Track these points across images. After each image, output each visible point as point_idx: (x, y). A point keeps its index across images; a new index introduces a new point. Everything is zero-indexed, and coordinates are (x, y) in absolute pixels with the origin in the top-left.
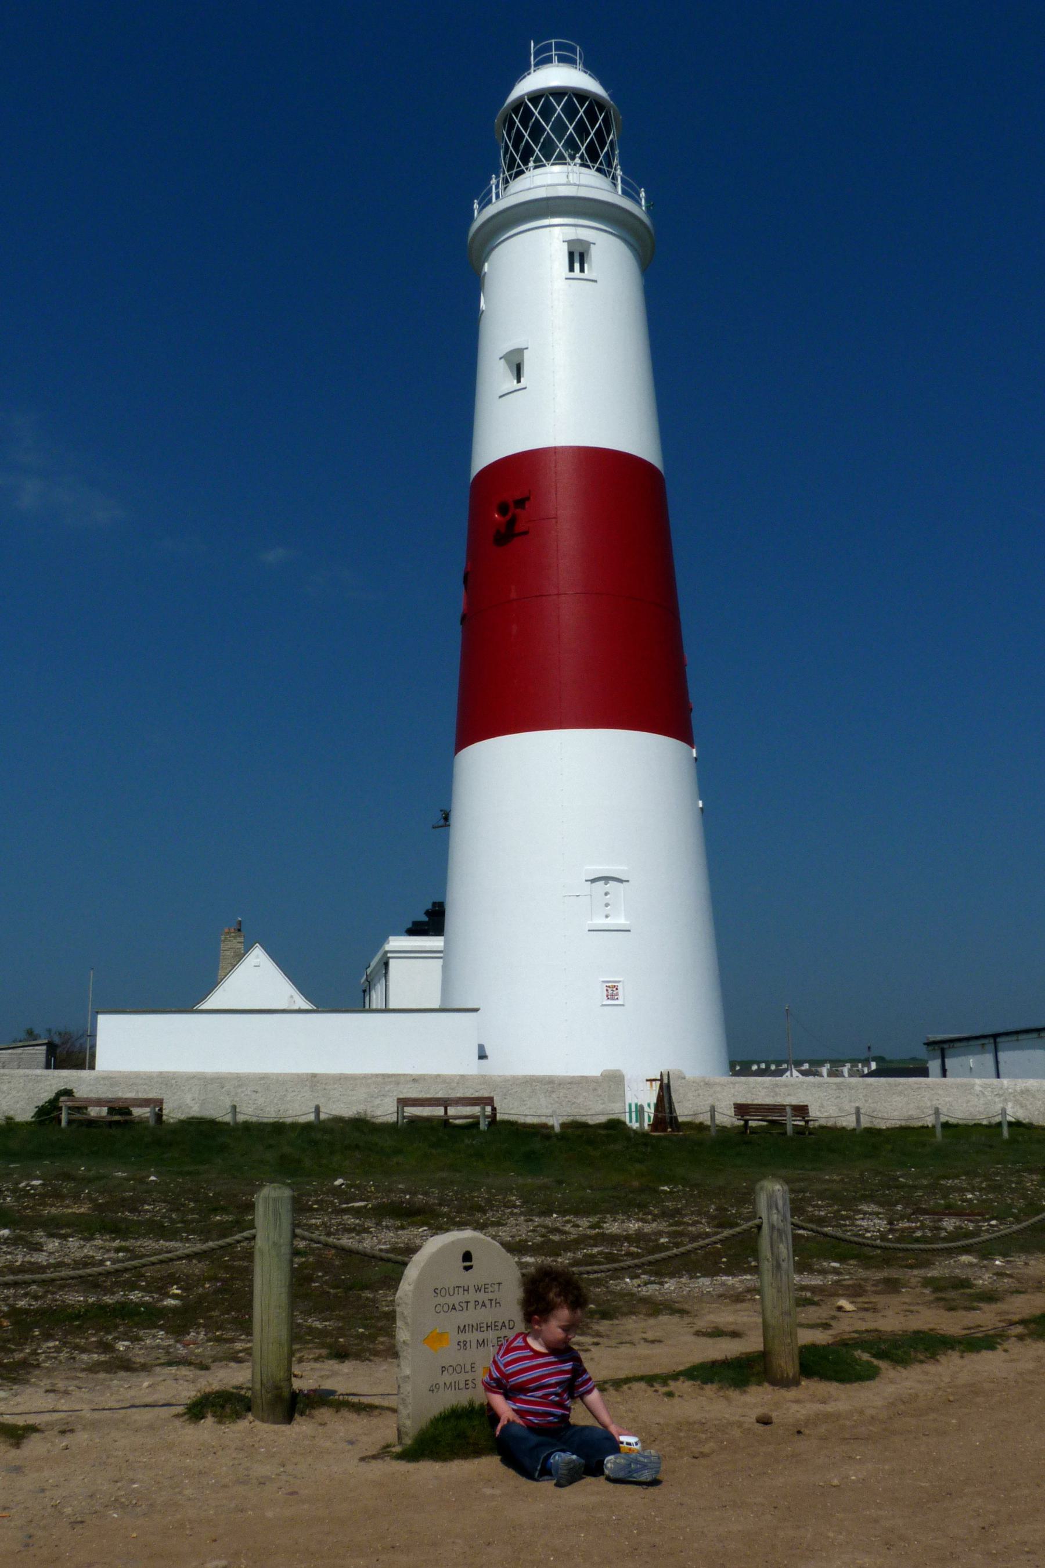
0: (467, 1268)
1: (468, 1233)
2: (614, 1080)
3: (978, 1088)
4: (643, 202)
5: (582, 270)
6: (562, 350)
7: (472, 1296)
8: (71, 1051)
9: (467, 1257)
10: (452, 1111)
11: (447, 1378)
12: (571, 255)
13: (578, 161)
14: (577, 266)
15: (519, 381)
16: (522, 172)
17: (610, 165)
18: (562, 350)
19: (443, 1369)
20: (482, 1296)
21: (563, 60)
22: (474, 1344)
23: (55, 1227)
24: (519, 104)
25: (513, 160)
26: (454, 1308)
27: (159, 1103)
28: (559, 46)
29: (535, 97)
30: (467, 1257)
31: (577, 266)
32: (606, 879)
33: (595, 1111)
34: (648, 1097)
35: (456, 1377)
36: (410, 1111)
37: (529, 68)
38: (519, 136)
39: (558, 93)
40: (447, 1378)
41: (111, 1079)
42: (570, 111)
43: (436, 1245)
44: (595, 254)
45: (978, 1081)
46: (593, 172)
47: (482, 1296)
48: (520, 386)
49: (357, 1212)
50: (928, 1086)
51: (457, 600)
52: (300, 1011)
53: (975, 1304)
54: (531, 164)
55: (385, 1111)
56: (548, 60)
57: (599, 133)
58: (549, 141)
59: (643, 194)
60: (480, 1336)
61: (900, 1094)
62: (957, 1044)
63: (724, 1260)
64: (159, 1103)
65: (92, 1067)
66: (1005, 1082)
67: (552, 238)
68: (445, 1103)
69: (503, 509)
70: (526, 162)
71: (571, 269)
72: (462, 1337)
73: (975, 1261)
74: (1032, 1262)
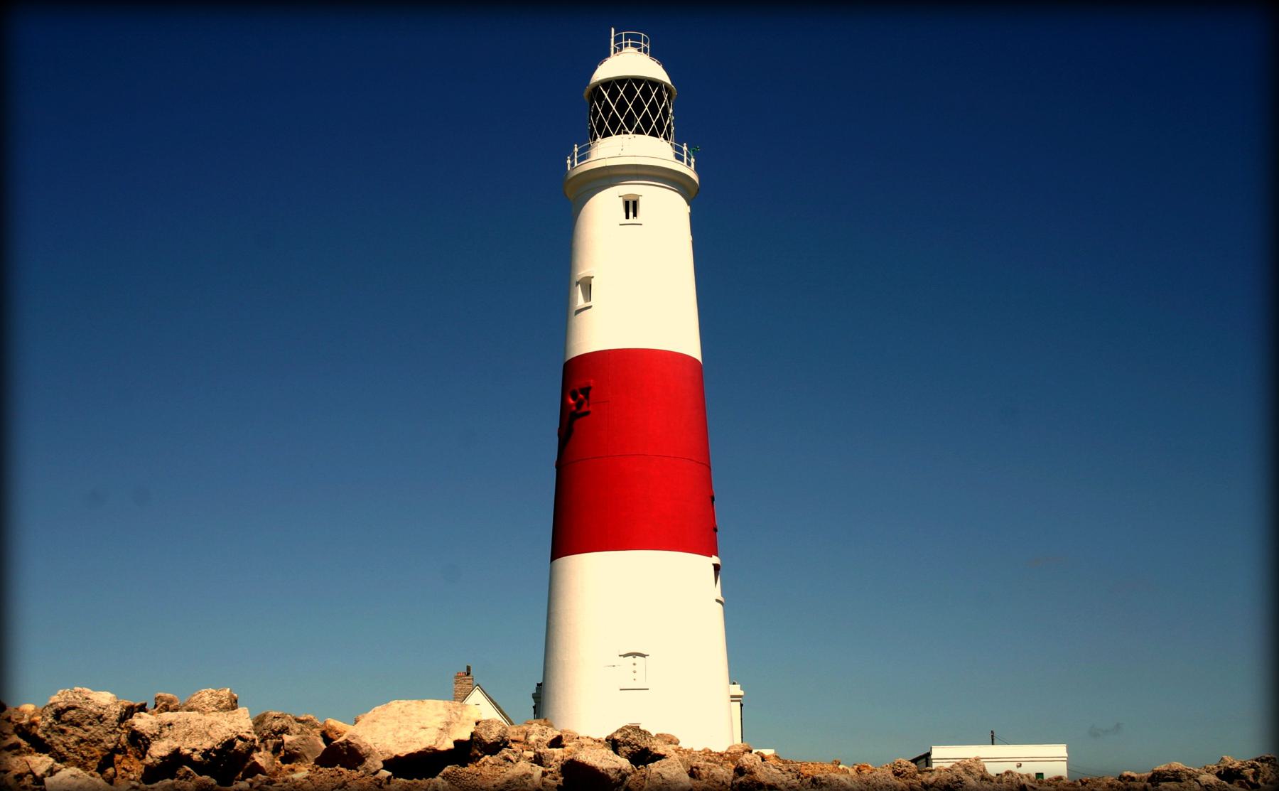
5: (635, 215)
6: (638, 275)
12: (627, 204)
14: (631, 214)
18: (638, 275)
31: (631, 214)
32: (634, 655)
37: (752, 781)
39: (621, 81)
48: (588, 304)
59: (685, 148)
63: (629, 62)
67: (603, 208)
69: (574, 396)
71: (627, 217)
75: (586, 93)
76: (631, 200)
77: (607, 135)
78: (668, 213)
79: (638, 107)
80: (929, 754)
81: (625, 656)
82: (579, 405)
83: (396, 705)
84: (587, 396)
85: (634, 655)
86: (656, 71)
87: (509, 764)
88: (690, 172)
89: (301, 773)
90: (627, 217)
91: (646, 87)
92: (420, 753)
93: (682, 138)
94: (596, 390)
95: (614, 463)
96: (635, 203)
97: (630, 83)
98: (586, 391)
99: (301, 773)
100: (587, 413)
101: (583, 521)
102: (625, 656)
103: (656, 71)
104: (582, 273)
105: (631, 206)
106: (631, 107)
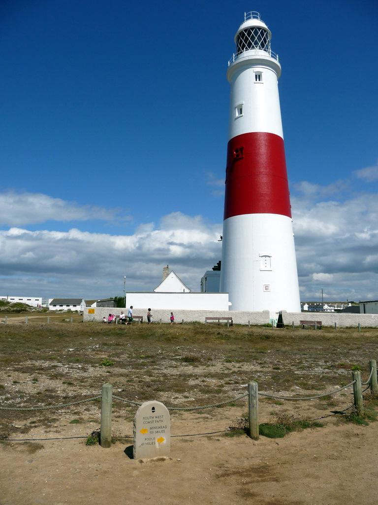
0: (153, 412)
1: (155, 402)
2: (267, 313)
3: (373, 317)
4: (278, 59)
5: (259, 80)
7: (155, 419)
8: (120, 302)
9: (153, 408)
10: (221, 321)
11: (146, 441)
12: (256, 76)
13: (258, 48)
14: (258, 80)
15: (241, 114)
16: (242, 52)
17: (268, 48)
18: (260, 105)
19: (146, 439)
20: (157, 419)
21: (254, 17)
22: (155, 432)
23: (93, 363)
25: (239, 49)
26: (149, 422)
28: (253, 14)
29: (246, 30)
30: (153, 408)
31: (258, 80)
32: (266, 256)
33: (262, 321)
34: (276, 318)
35: (149, 441)
36: (209, 321)
38: (241, 41)
39: (252, 28)
40: (146, 441)
42: (256, 33)
43: (146, 405)
44: (263, 76)
45: (373, 315)
46: (263, 51)
47: (157, 419)
48: (241, 115)
49: (176, 360)
52: (184, 293)
54: (245, 50)
56: (250, 18)
58: (244, 45)
59: (277, 56)
60: (156, 430)
61: (349, 318)
62: (368, 303)
67: (250, 73)
68: (219, 319)
70: (243, 49)
71: (256, 80)
72: (151, 430)
74: (218, 487)
75: (238, 33)
76: (258, 74)
77: (247, 49)
78: (270, 78)
79: (259, 39)
81: (262, 257)
82: (238, 155)
84: (242, 152)
85: (266, 256)
86: (263, 25)
87: (253, 459)
88: (277, 62)
89: (128, 502)
90: (256, 80)
91: (262, 32)
93: (275, 52)
94: (242, 148)
95: (250, 180)
96: (259, 76)
97: (256, 29)
98: (241, 149)
99: (128, 502)
100: (242, 158)
101: (239, 200)
102: (262, 257)
103: (263, 25)
104: (237, 103)
105: (258, 77)
106: (248, 39)
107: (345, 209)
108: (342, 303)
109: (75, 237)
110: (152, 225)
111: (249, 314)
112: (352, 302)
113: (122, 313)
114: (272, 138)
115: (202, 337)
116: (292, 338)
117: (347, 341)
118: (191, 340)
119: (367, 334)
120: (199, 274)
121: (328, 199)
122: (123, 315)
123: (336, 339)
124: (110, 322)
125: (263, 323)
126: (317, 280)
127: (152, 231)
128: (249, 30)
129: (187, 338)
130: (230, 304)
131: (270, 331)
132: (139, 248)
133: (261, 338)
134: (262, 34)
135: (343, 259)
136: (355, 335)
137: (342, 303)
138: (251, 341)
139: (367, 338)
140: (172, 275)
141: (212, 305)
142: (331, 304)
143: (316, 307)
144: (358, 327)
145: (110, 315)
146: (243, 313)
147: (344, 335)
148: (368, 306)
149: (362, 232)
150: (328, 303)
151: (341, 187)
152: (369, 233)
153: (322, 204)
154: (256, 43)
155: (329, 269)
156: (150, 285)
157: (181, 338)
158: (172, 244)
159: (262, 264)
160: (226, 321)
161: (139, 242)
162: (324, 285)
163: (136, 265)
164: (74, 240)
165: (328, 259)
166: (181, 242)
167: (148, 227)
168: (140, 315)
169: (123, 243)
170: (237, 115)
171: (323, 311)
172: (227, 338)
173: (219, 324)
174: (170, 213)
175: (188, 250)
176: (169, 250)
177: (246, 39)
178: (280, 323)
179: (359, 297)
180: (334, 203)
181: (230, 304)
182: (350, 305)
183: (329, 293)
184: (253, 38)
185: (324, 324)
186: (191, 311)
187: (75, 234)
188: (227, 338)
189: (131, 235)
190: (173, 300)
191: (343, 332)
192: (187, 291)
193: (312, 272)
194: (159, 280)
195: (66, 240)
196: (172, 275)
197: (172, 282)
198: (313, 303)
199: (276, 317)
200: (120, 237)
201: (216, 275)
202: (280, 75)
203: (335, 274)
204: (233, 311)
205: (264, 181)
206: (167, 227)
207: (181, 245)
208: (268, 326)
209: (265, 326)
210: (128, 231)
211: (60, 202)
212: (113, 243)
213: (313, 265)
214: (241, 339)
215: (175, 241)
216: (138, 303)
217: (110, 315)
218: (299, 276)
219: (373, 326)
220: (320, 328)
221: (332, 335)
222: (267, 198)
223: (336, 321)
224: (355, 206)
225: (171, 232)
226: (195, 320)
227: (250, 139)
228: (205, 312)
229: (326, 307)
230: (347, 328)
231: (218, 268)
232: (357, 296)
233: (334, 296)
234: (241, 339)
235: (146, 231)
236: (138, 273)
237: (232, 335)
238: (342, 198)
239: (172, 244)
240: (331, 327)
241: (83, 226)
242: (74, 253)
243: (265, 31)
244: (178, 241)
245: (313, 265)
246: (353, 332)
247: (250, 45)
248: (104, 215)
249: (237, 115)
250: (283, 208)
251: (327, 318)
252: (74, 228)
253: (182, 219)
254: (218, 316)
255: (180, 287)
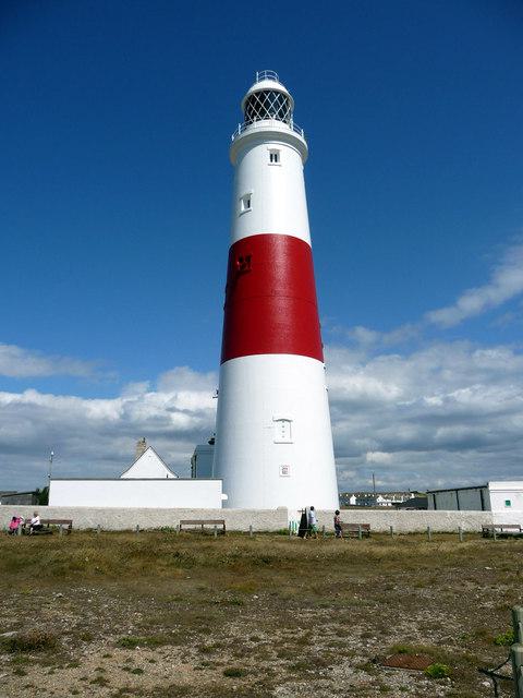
2: (283, 511)
6: (276, 196)
8: (41, 497)
16: (251, 123)
18: (276, 196)
24: (252, 99)
27: (70, 522)
28: (268, 73)
29: (257, 94)
32: (283, 420)
33: (275, 526)
36: (184, 527)
38: (251, 108)
39: (267, 91)
41: (54, 511)
44: (282, 156)
50: (426, 514)
51: (221, 298)
52: (167, 479)
53: (344, 416)
55: (174, 524)
57: (284, 107)
64: (70, 522)
65: (47, 504)
66: (461, 512)
67: (261, 152)
68: (202, 523)
69: (241, 261)
73: (357, 441)
75: (246, 98)
78: (292, 163)
79: (277, 105)
80: (486, 487)
82: (242, 267)
83: (177, 368)
86: (281, 88)
88: (301, 138)
92: (304, 165)
94: (250, 256)
95: (259, 306)
98: (248, 258)
101: (245, 332)
103: (281, 88)
104: (243, 193)
105: (274, 157)
106: (260, 105)
107: (409, 365)
108: (402, 494)
109: (39, 396)
110: (146, 384)
111: (255, 513)
112: (415, 493)
113: (35, 516)
114: (294, 243)
115: (136, 563)
116: (314, 560)
117: (407, 563)
118: (110, 573)
119: (444, 547)
120: (185, 455)
121: (388, 351)
122: (38, 518)
123: (392, 558)
124: (12, 532)
125: (277, 529)
126: (372, 462)
127: (146, 392)
128: (262, 94)
129: (105, 568)
130: (225, 497)
131: (286, 545)
132: (125, 416)
133: (255, 563)
134: (281, 100)
135: (406, 433)
136: (424, 549)
137: (402, 494)
138: (233, 569)
139: (444, 555)
140: (150, 452)
141: (199, 499)
142: (387, 495)
143: (366, 501)
144: (427, 532)
145: (14, 519)
146: (246, 512)
147: (405, 550)
148: (439, 497)
149: (433, 395)
150: (382, 494)
151: (400, 318)
152: (442, 396)
153: (381, 358)
154: (271, 111)
155: (388, 447)
156: (113, 467)
157: (90, 569)
158: (173, 410)
159: (278, 432)
160: (212, 527)
161: (123, 407)
162: (383, 468)
163: (118, 442)
164: (32, 405)
165: (385, 433)
166: (187, 408)
167: (141, 387)
168: (68, 518)
169: (103, 409)
170: (243, 209)
171: (379, 507)
172: (190, 563)
173: (204, 533)
174: (172, 368)
175: (197, 420)
176: (169, 419)
177: (258, 106)
178: (305, 524)
179: (427, 485)
180: (397, 356)
181: (225, 497)
182: (413, 496)
183: (386, 480)
184: (267, 105)
185: (375, 527)
186: (159, 511)
187: (31, 396)
188: (190, 563)
189: (114, 398)
190: (151, 495)
191: (403, 542)
192: (171, 476)
193: (366, 451)
194: (131, 461)
195: (18, 405)
196: (150, 452)
197: (149, 464)
198: (363, 494)
199: (299, 518)
200: (97, 401)
201: (207, 455)
202: (306, 158)
203: (396, 454)
204: (229, 510)
205: (282, 305)
206: (166, 389)
207: (186, 412)
208: (285, 533)
209: (279, 533)
210: (109, 393)
211: (15, 350)
212: (90, 410)
213: (366, 442)
214: (216, 566)
215: (177, 407)
216: (74, 499)
217: (14, 519)
218: (336, 456)
219: (450, 530)
220: (367, 535)
221: (384, 550)
222: (286, 332)
223: (393, 524)
224: (425, 360)
225: (171, 395)
226: (164, 525)
227: (261, 243)
228: (183, 511)
229: (380, 499)
230: (410, 533)
231: (212, 442)
232: (423, 484)
233: (393, 484)
234: (216, 566)
235: (137, 393)
236: (121, 453)
237: (201, 557)
238: (407, 350)
239: (173, 410)
240: (385, 533)
241: (42, 385)
242: (28, 424)
243: (285, 97)
244: (181, 407)
245: (366, 442)
246: (420, 541)
247: (263, 113)
248: (79, 369)
249: (243, 209)
250: (308, 344)
251: (377, 520)
252: (32, 388)
253: (189, 375)
254: (203, 519)
255: (160, 470)
